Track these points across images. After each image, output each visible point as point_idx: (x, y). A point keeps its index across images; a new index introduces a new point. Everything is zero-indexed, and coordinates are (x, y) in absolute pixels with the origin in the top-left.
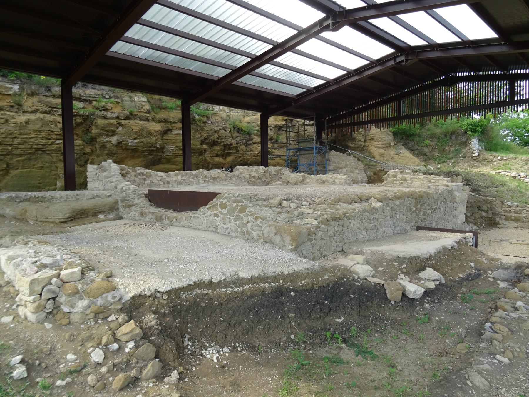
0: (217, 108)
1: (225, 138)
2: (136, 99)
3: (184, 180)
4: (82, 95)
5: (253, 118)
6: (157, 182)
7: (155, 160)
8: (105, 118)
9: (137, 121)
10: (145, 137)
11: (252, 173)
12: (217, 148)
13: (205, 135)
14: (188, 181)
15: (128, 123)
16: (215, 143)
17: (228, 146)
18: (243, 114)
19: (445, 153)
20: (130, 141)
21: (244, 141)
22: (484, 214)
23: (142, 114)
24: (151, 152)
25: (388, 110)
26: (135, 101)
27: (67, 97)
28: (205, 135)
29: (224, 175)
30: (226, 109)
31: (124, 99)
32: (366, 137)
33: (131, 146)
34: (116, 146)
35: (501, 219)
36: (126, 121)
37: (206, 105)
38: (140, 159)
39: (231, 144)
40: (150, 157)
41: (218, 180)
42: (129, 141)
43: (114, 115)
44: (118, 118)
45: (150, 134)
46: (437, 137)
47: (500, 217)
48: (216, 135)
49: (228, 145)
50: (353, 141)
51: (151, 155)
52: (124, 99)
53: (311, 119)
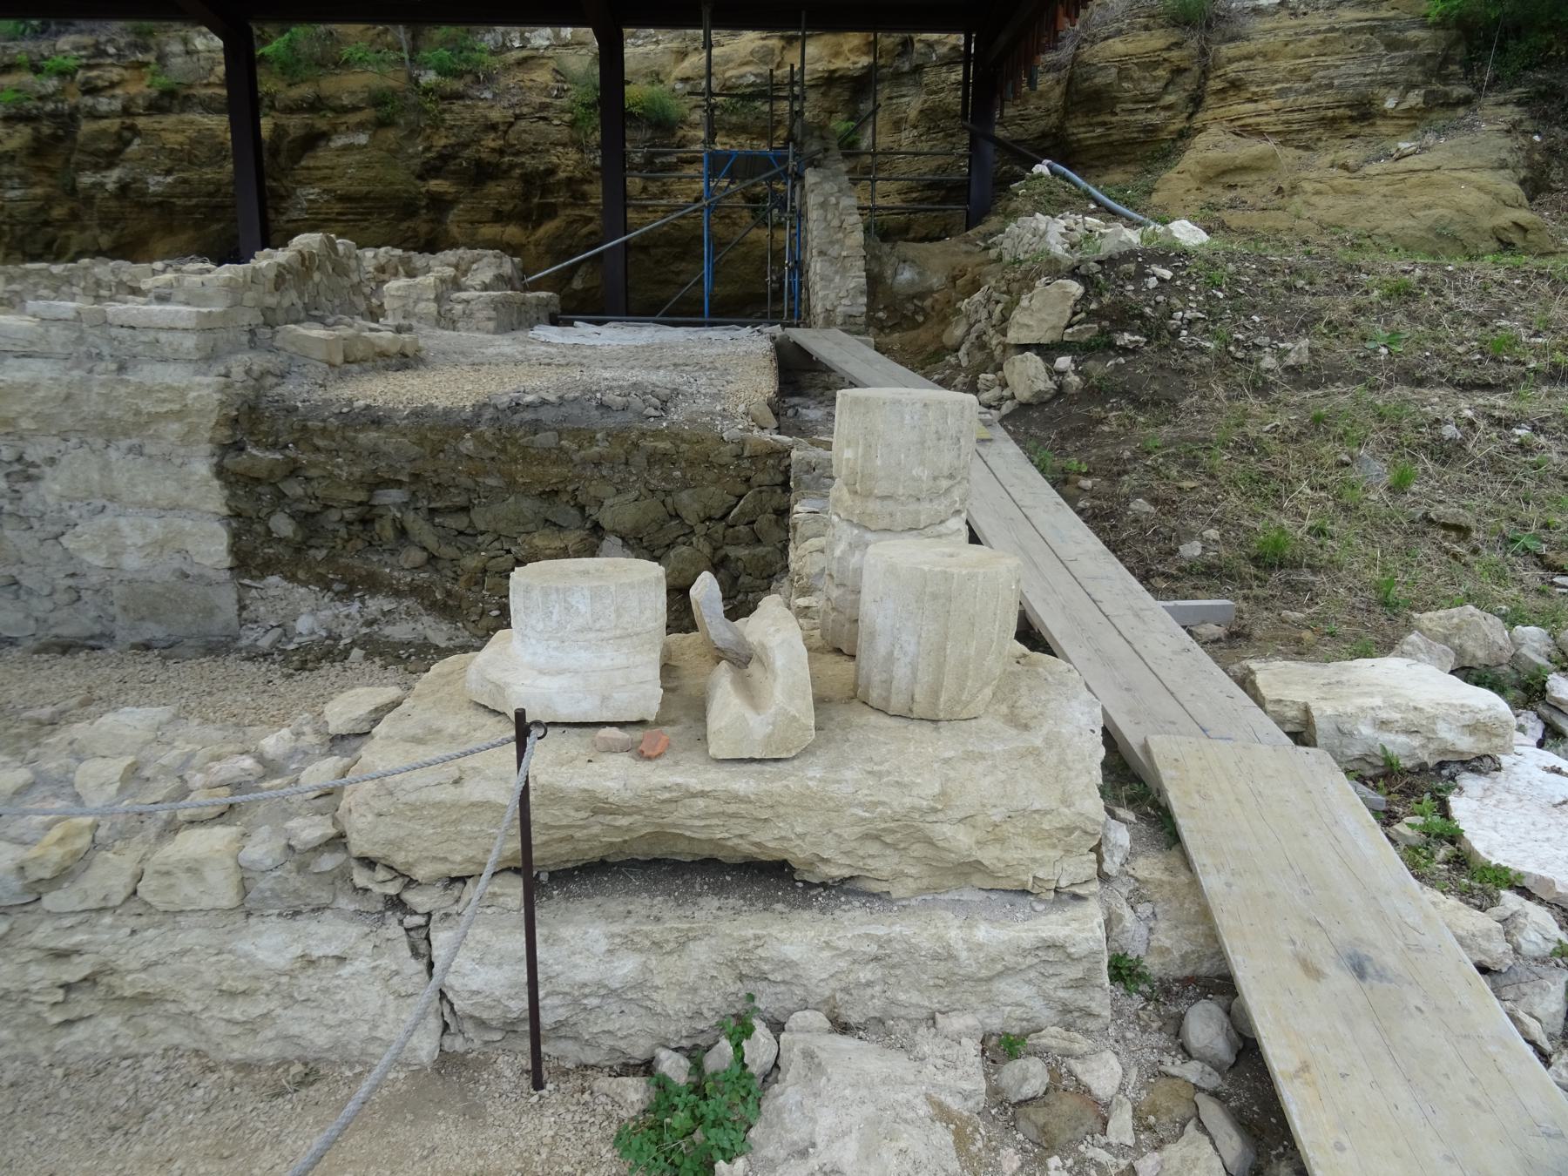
0: (541, 37)
1: (533, 150)
3: (16, 292)
10: (201, 166)
12: (497, 189)
13: (440, 142)
15: (156, 126)
16: (483, 173)
17: (540, 181)
18: (675, 45)
20: (152, 180)
23: (209, 91)
28: (443, 142)
31: (168, 49)
33: (155, 194)
37: (500, 29)
39: (551, 171)
40: (216, 227)
42: (150, 181)
43: (117, 105)
44: (126, 111)
48: (491, 141)
50: (1099, 112)
51: (219, 221)
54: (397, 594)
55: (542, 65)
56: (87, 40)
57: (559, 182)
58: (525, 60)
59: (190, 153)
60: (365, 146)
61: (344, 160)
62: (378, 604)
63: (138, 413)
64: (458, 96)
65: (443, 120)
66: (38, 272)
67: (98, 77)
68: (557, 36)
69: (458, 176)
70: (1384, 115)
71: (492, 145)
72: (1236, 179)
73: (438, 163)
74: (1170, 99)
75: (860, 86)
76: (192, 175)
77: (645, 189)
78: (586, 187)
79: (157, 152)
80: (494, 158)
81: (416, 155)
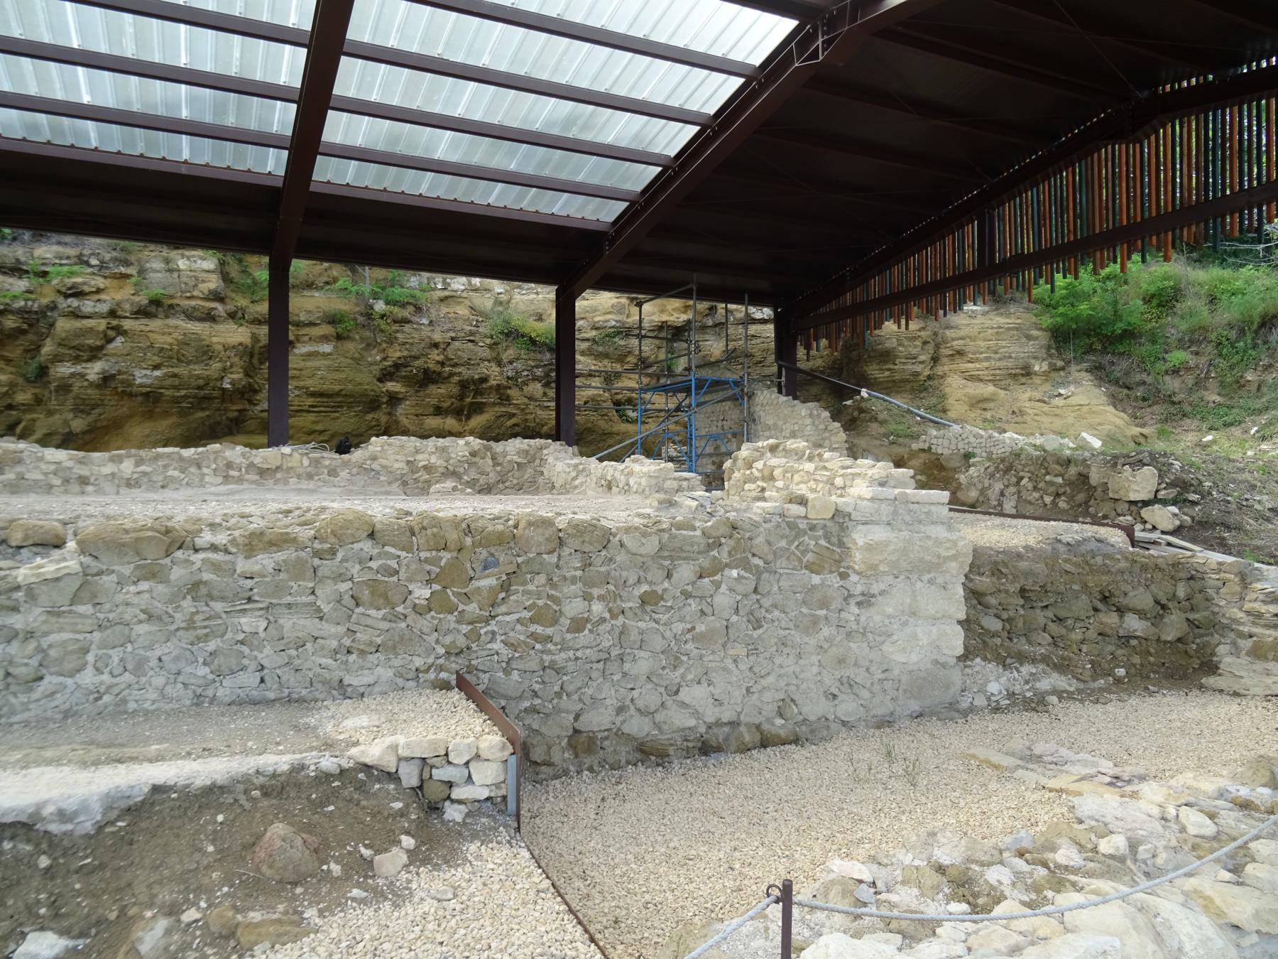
0: (459, 283)
1: (467, 363)
2: (182, 264)
3: (145, 474)
4: (23, 259)
5: (533, 302)
6: (40, 477)
7: (219, 423)
8: (76, 315)
9: (172, 322)
10: (189, 363)
11: (419, 457)
12: (438, 392)
13: (396, 354)
14: (158, 478)
15: (143, 328)
16: (428, 378)
17: (474, 386)
19: (1243, 392)
20: (137, 373)
21: (539, 372)
22: (1134, 624)
23: (193, 303)
24: (201, 401)
25: (964, 247)
26: (179, 271)
27: (279, 288)
28: (398, 354)
29: (306, 462)
30: (498, 286)
32: (937, 346)
33: (141, 385)
34: (98, 386)
35: (1236, 651)
36: (138, 322)
37: (426, 275)
38: (169, 422)
39: (484, 380)
41: (279, 475)
43: (104, 308)
44: (112, 314)
45: (206, 353)
46: (1213, 337)
47: (1234, 644)
48: (435, 355)
49: (474, 381)
50: (886, 362)
51: (203, 409)
52: (148, 265)
53: (758, 301)
54: (1034, 661)
55: (460, 303)
56: (72, 252)
57: (491, 387)
58: (447, 297)
59: (178, 352)
60: (330, 354)
61: (309, 364)
62: (1026, 669)
63: (939, 557)
64: (408, 321)
65: (396, 338)
66: (169, 455)
67: (85, 283)
68: (470, 283)
69: (408, 380)
70: (1036, 374)
71: (438, 358)
72: (985, 406)
73: (392, 370)
74: (922, 358)
75: (677, 333)
76: (182, 370)
77: (545, 394)
78: (509, 391)
79: (144, 350)
80: (438, 368)
81: (375, 363)
